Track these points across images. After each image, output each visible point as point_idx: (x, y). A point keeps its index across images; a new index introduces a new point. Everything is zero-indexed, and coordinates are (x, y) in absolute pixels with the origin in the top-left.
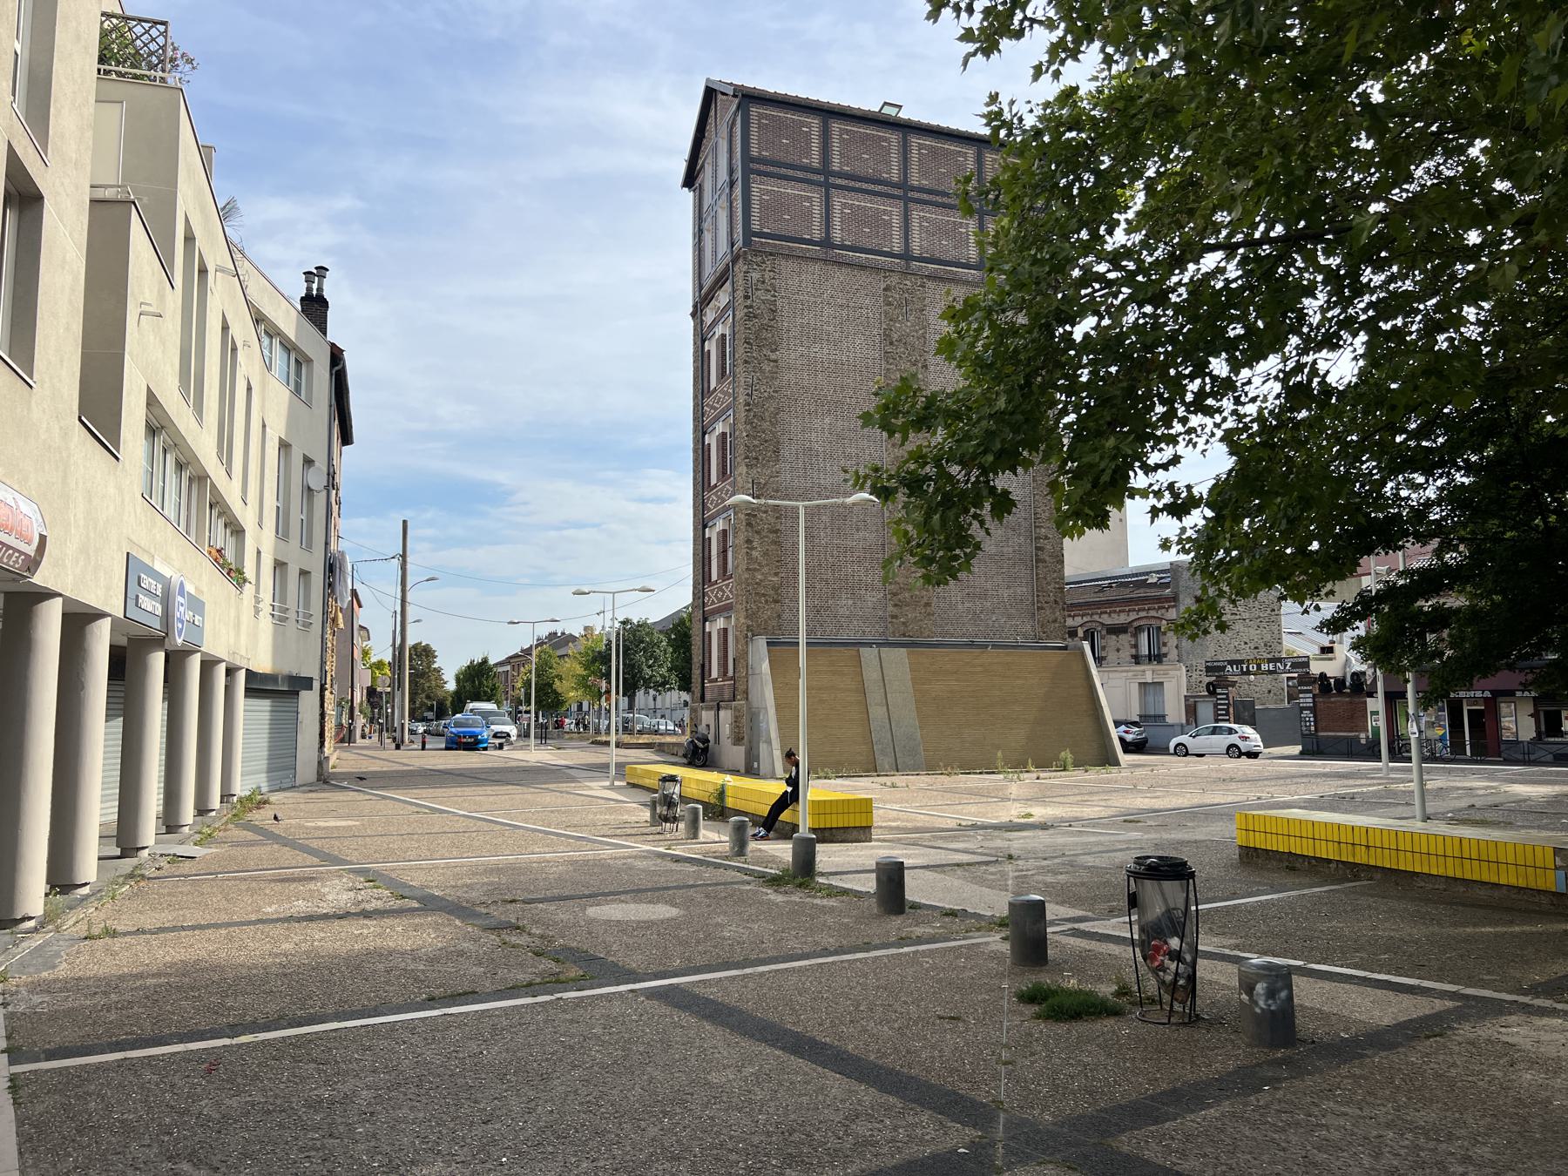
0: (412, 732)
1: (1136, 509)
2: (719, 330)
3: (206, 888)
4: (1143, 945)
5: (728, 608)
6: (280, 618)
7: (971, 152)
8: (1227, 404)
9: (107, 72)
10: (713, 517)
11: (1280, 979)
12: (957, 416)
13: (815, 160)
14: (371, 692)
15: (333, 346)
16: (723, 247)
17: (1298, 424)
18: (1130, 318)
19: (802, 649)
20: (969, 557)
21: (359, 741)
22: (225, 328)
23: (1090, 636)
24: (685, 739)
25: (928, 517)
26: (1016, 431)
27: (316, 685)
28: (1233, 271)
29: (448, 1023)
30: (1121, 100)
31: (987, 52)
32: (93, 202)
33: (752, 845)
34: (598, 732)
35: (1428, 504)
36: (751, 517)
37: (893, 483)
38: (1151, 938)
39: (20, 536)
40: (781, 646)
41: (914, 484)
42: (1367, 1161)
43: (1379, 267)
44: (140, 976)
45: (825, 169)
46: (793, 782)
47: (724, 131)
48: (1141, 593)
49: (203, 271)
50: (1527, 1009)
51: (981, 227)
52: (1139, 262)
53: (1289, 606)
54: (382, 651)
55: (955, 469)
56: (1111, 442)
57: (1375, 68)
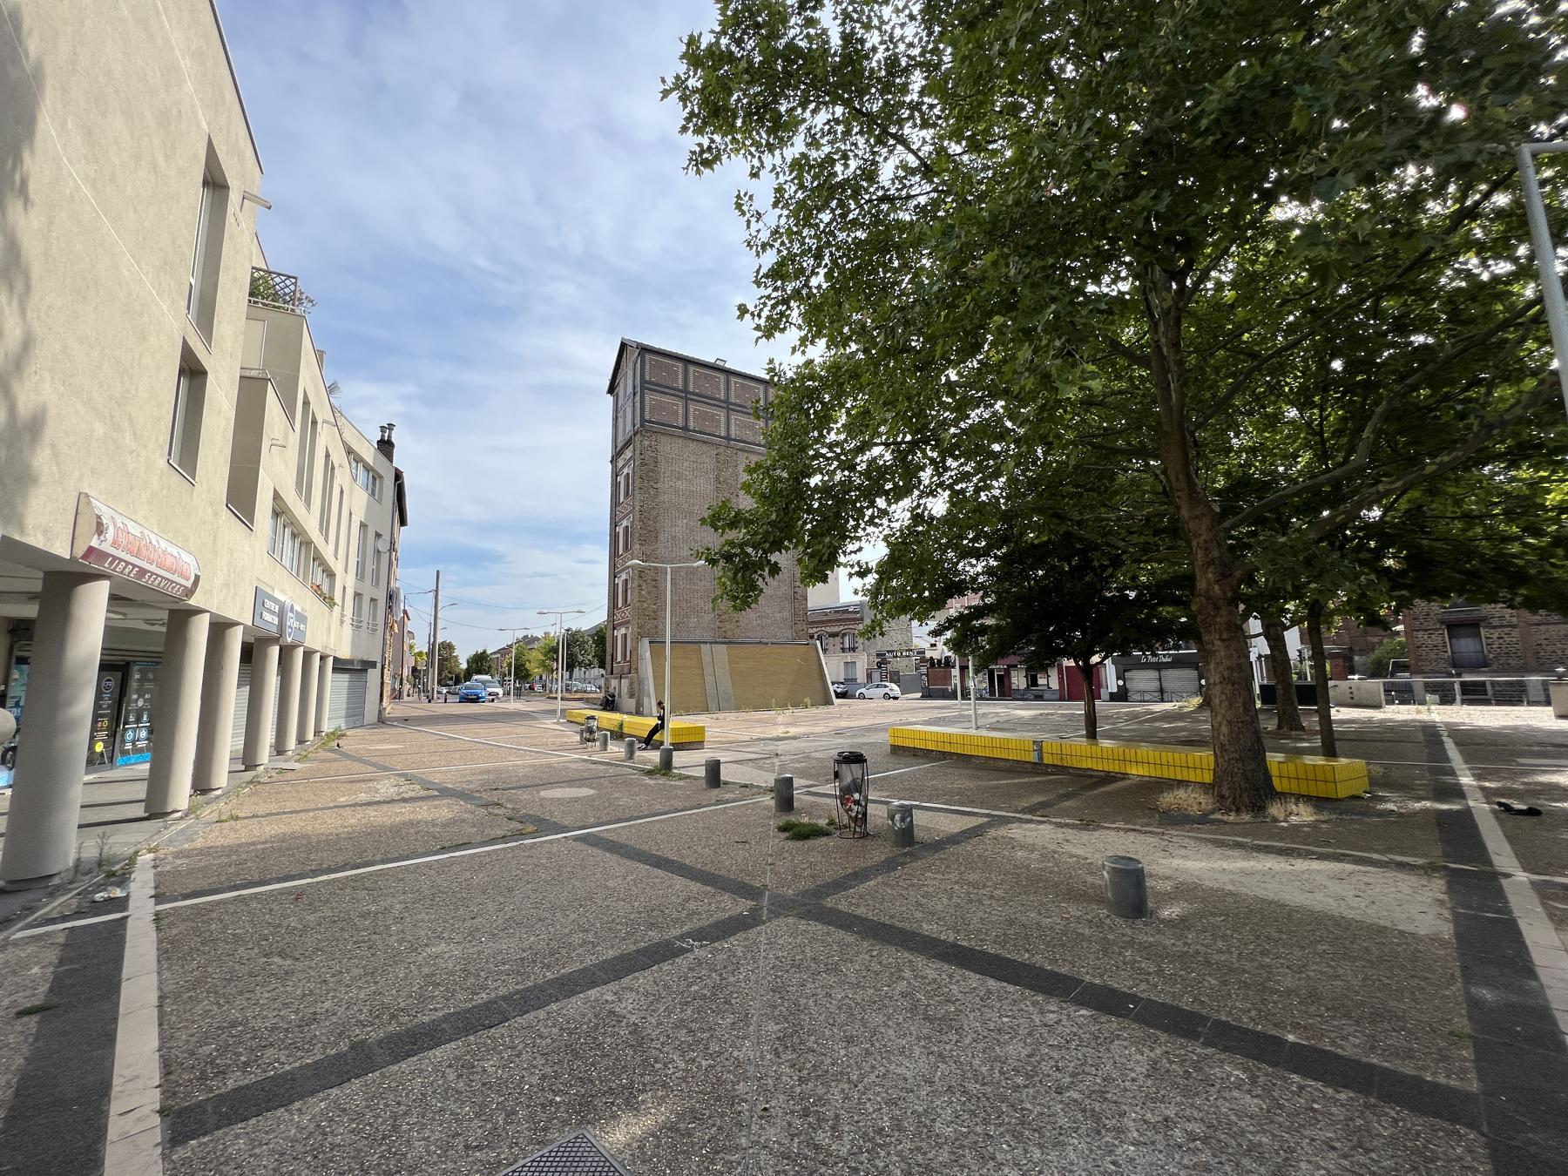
0: (439, 693)
1: (842, 572)
2: (626, 471)
3: (301, 788)
4: (841, 798)
5: (628, 622)
6: (357, 625)
7: (761, 387)
8: (885, 522)
9: (255, 302)
10: (620, 572)
11: (907, 812)
12: (752, 522)
13: (680, 385)
14: (414, 670)
15: (396, 469)
16: (629, 427)
17: (918, 533)
18: (838, 477)
19: (668, 640)
20: (757, 596)
21: (406, 698)
22: (328, 456)
23: (819, 638)
24: (601, 696)
25: (735, 575)
26: (781, 531)
27: (379, 666)
28: (888, 456)
29: (453, 861)
30: (834, 368)
31: (768, 337)
32: (241, 377)
33: (638, 753)
34: (551, 691)
35: (978, 575)
36: (641, 572)
37: (717, 557)
38: (845, 794)
39: (181, 575)
40: (657, 644)
41: (728, 557)
42: (945, 901)
43: (956, 458)
44: (254, 843)
45: (685, 390)
46: (661, 718)
47: (631, 366)
48: (845, 616)
49: (314, 422)
50: (1020, 820)
51: (796, 192)
52: (843, 449)
53: (915, 623)
54: (422, 645)
55: (749, 550)
56: (828, 540)
57: (955, 364)
